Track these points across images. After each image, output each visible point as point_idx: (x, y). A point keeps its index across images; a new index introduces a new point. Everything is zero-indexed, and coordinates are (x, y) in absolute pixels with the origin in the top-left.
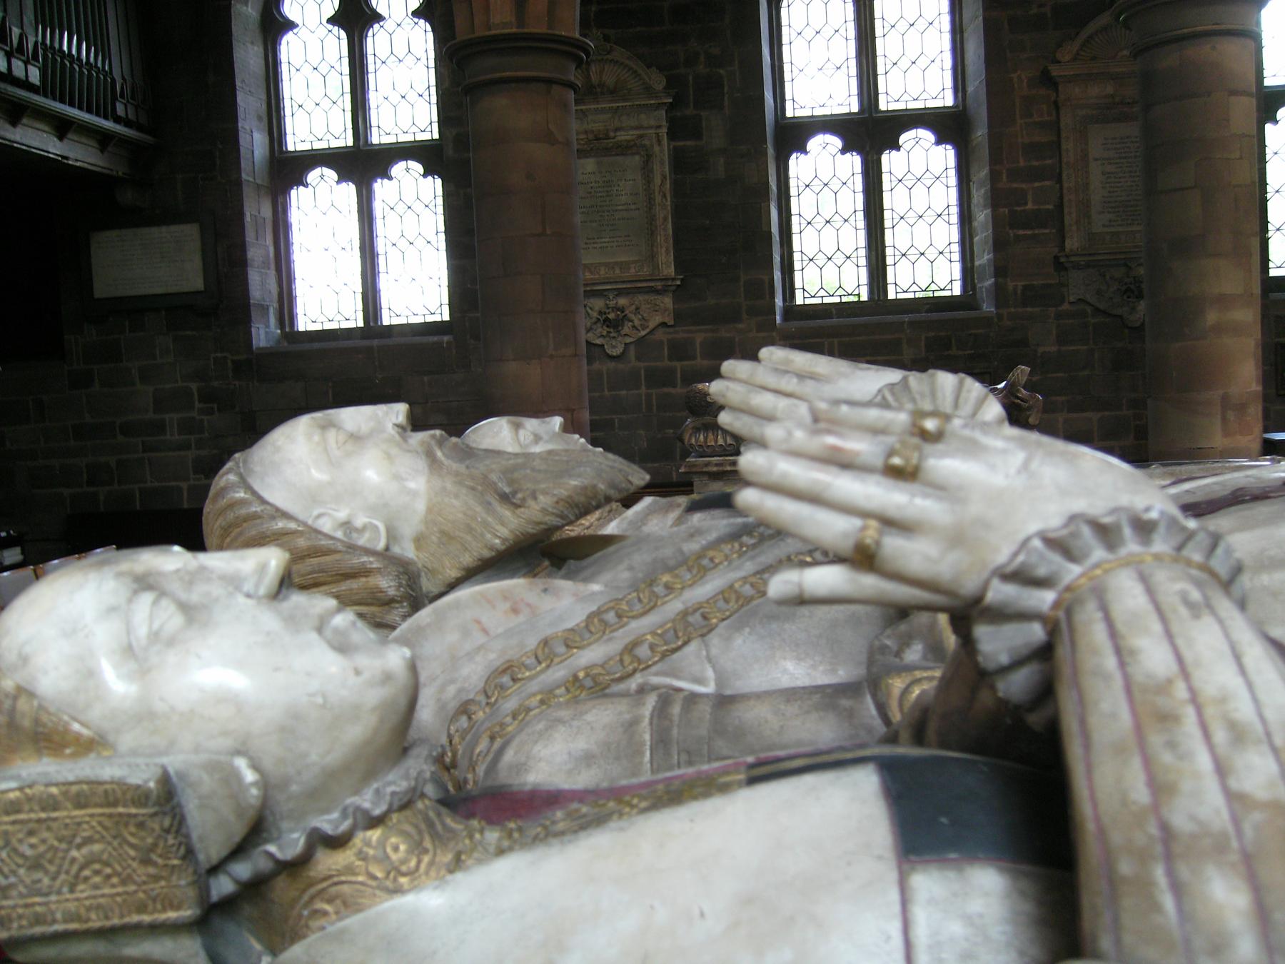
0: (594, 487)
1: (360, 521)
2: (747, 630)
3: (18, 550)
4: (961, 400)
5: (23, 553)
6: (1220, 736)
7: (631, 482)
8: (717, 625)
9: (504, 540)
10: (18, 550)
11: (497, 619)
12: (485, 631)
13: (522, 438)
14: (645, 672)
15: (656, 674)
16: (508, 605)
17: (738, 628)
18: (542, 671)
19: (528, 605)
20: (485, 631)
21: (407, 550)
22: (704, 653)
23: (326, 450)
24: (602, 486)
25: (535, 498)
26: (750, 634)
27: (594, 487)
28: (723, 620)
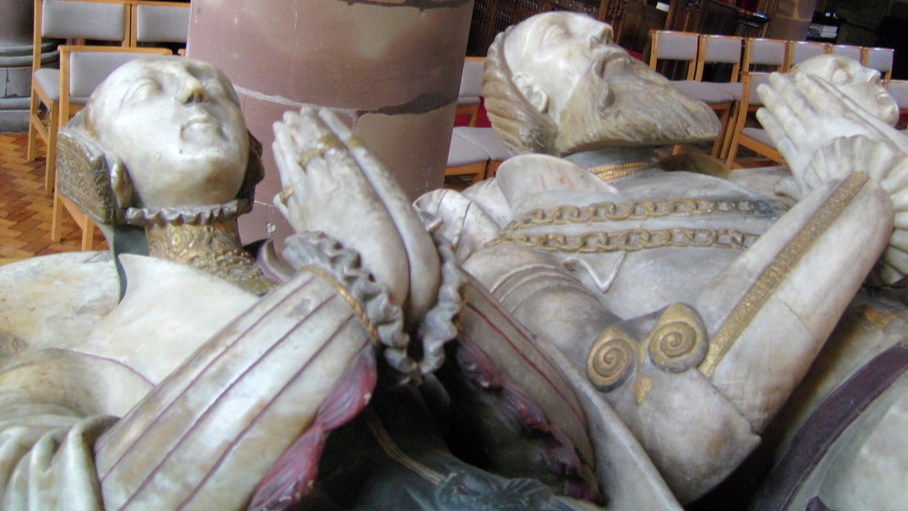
0: (655, 125)
1: (536, 89)
2: (652, 262)
3: (835, 29)
4: (892, 173)
5: (838, 32)
6: (213, 370)
7: (688, 133)
8: (639, 250)
9: (595, 136)
10: (835, 29)
11: (551, 180)
12: (544, 185)
13: (835, 77)
14: (582, 255)
15: (586, 259)
16: (559, 175)
17: (648, 258)
18: (544, 224)
19: (570, 181)
20: (544, 185)
21: (556, 118)
22: (620, 261)
23: (542, 38)
24: (659, 127)
25: (617, 116)
26: (651, 265)
27: (655, 125)
28: (645, 248)
